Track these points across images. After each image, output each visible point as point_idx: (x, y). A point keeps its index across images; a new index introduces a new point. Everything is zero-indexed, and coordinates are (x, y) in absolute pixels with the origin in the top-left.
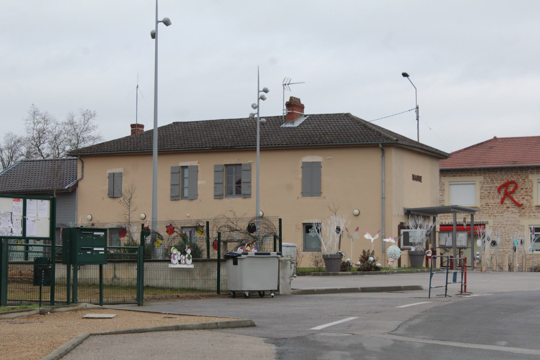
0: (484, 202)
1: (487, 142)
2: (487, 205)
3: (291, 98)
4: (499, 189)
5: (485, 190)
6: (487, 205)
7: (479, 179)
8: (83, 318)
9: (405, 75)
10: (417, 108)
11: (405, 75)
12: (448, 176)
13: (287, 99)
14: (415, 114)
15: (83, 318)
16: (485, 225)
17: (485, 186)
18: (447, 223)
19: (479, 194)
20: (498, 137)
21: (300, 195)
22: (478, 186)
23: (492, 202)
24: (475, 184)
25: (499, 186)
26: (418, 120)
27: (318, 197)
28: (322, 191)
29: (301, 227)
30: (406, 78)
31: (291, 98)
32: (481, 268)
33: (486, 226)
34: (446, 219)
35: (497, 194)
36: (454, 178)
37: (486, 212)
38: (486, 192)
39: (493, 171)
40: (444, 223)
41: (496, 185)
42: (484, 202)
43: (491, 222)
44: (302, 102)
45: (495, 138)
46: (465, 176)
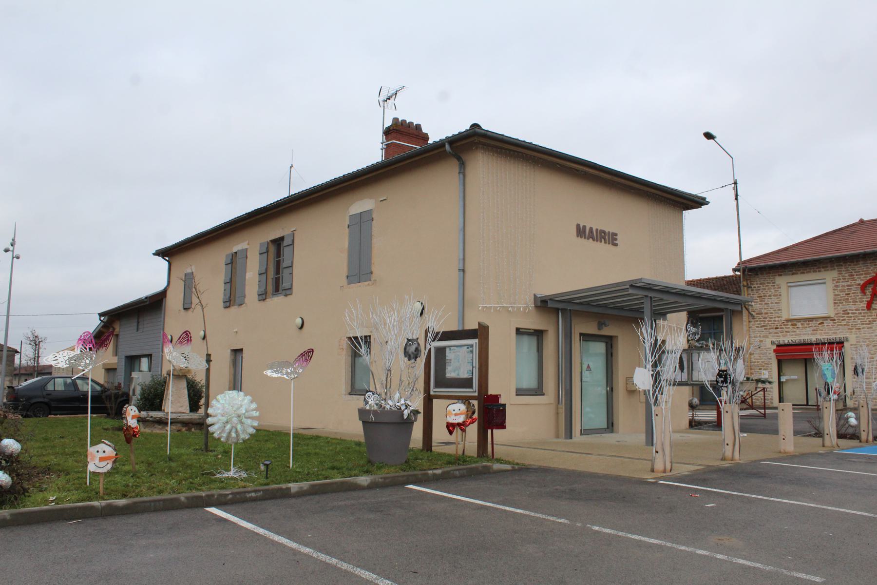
0: (840, 308)
1: (848, 227)
2: (845, 312)
3: (395, 120)
4: (863, 288)
5: (842, 291)
6: (845, 312)
7: (830, 276)
8: (203, 474)
9: (709, 136)
10: (735, 183)
11: (709, 136)
12: (786, 275)
13: (388, 123)
14: (733, 193)
15: (203, 474)
16: (843, 343)
17: (841, 284)
18: (786, 342)
19: (831, 296)
20: (865, 219)
21: (344, 281)
22: (830, 285)
23: (853, 307)
24: (825, 283)
25: (862, 282)
26: (736, 199)
27: (367, 283)
28: (374, 269)
29: (345, 343)
30: (712, 141)
31: (395, 120)
32: (652, 461)
33: (846, 344)
34: (784, 336)
35: (860, 295)
36: (795, 276)
37: (844, 323)
38: (842, 294)
39: (852, 262)
40: (782, 343)
41: (857, 282)
42: (840, 308)
43: (852, 338)
44: (424, 131)
45: (862, 221)
46: (809, 272)
